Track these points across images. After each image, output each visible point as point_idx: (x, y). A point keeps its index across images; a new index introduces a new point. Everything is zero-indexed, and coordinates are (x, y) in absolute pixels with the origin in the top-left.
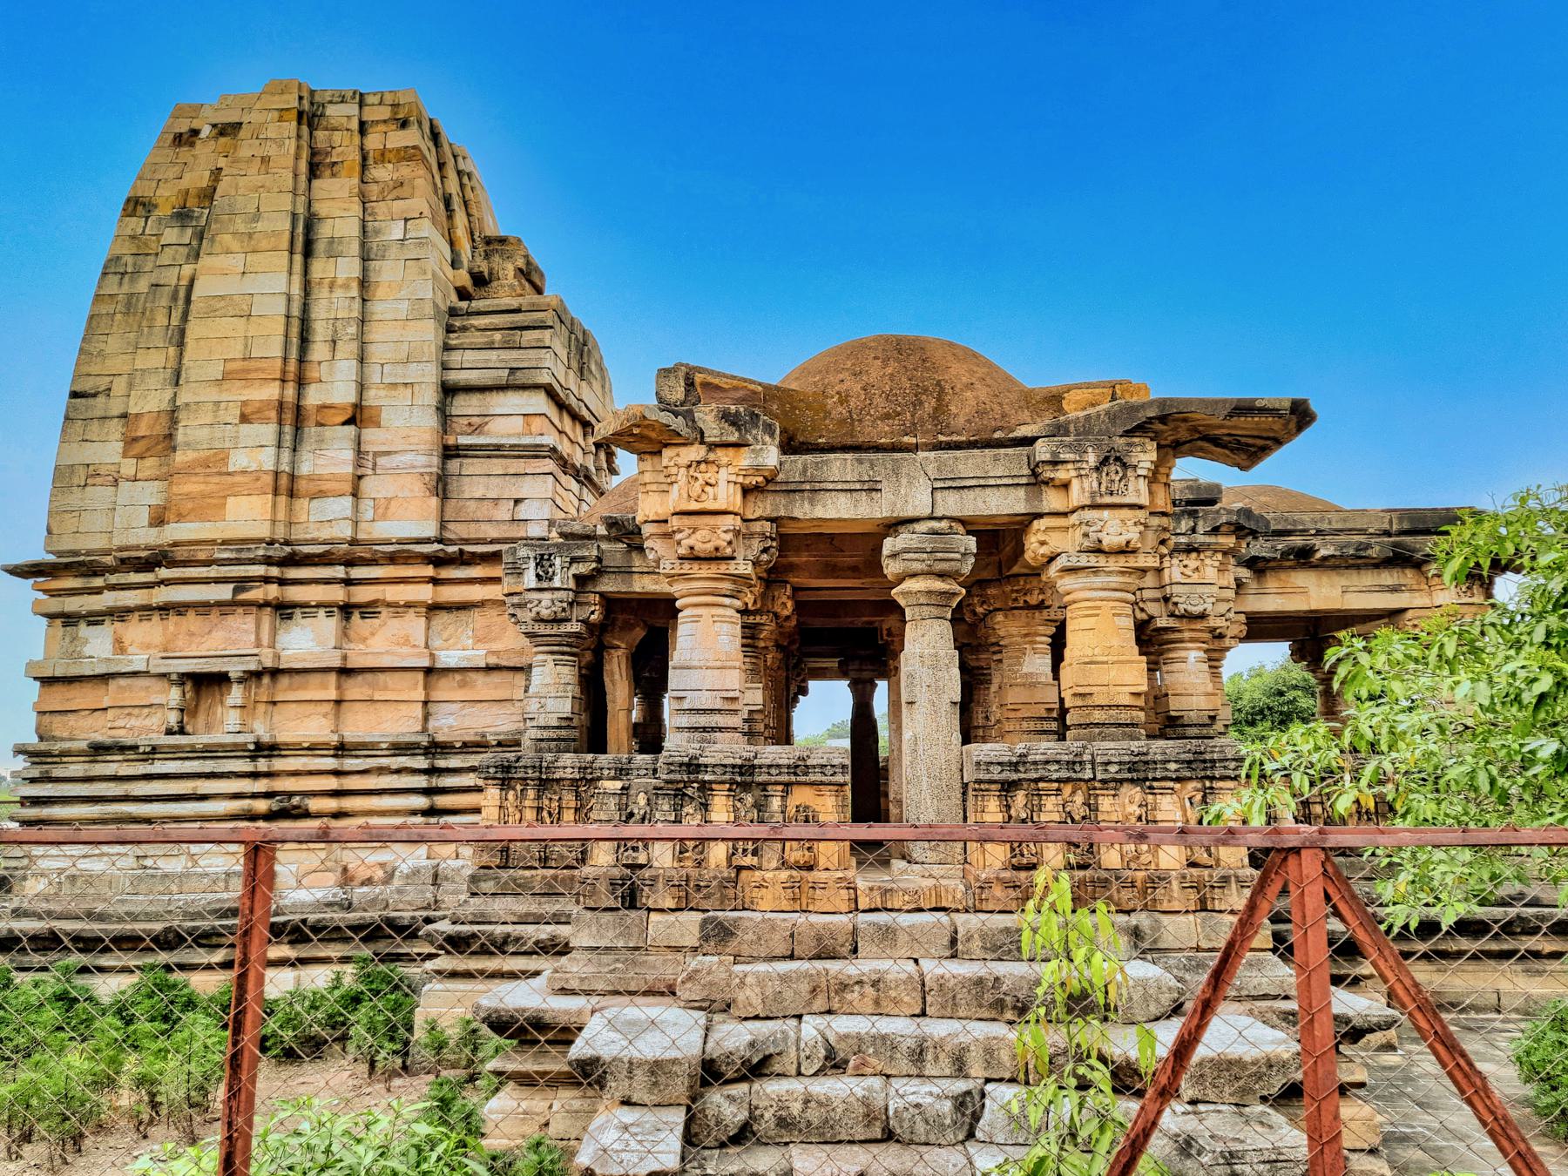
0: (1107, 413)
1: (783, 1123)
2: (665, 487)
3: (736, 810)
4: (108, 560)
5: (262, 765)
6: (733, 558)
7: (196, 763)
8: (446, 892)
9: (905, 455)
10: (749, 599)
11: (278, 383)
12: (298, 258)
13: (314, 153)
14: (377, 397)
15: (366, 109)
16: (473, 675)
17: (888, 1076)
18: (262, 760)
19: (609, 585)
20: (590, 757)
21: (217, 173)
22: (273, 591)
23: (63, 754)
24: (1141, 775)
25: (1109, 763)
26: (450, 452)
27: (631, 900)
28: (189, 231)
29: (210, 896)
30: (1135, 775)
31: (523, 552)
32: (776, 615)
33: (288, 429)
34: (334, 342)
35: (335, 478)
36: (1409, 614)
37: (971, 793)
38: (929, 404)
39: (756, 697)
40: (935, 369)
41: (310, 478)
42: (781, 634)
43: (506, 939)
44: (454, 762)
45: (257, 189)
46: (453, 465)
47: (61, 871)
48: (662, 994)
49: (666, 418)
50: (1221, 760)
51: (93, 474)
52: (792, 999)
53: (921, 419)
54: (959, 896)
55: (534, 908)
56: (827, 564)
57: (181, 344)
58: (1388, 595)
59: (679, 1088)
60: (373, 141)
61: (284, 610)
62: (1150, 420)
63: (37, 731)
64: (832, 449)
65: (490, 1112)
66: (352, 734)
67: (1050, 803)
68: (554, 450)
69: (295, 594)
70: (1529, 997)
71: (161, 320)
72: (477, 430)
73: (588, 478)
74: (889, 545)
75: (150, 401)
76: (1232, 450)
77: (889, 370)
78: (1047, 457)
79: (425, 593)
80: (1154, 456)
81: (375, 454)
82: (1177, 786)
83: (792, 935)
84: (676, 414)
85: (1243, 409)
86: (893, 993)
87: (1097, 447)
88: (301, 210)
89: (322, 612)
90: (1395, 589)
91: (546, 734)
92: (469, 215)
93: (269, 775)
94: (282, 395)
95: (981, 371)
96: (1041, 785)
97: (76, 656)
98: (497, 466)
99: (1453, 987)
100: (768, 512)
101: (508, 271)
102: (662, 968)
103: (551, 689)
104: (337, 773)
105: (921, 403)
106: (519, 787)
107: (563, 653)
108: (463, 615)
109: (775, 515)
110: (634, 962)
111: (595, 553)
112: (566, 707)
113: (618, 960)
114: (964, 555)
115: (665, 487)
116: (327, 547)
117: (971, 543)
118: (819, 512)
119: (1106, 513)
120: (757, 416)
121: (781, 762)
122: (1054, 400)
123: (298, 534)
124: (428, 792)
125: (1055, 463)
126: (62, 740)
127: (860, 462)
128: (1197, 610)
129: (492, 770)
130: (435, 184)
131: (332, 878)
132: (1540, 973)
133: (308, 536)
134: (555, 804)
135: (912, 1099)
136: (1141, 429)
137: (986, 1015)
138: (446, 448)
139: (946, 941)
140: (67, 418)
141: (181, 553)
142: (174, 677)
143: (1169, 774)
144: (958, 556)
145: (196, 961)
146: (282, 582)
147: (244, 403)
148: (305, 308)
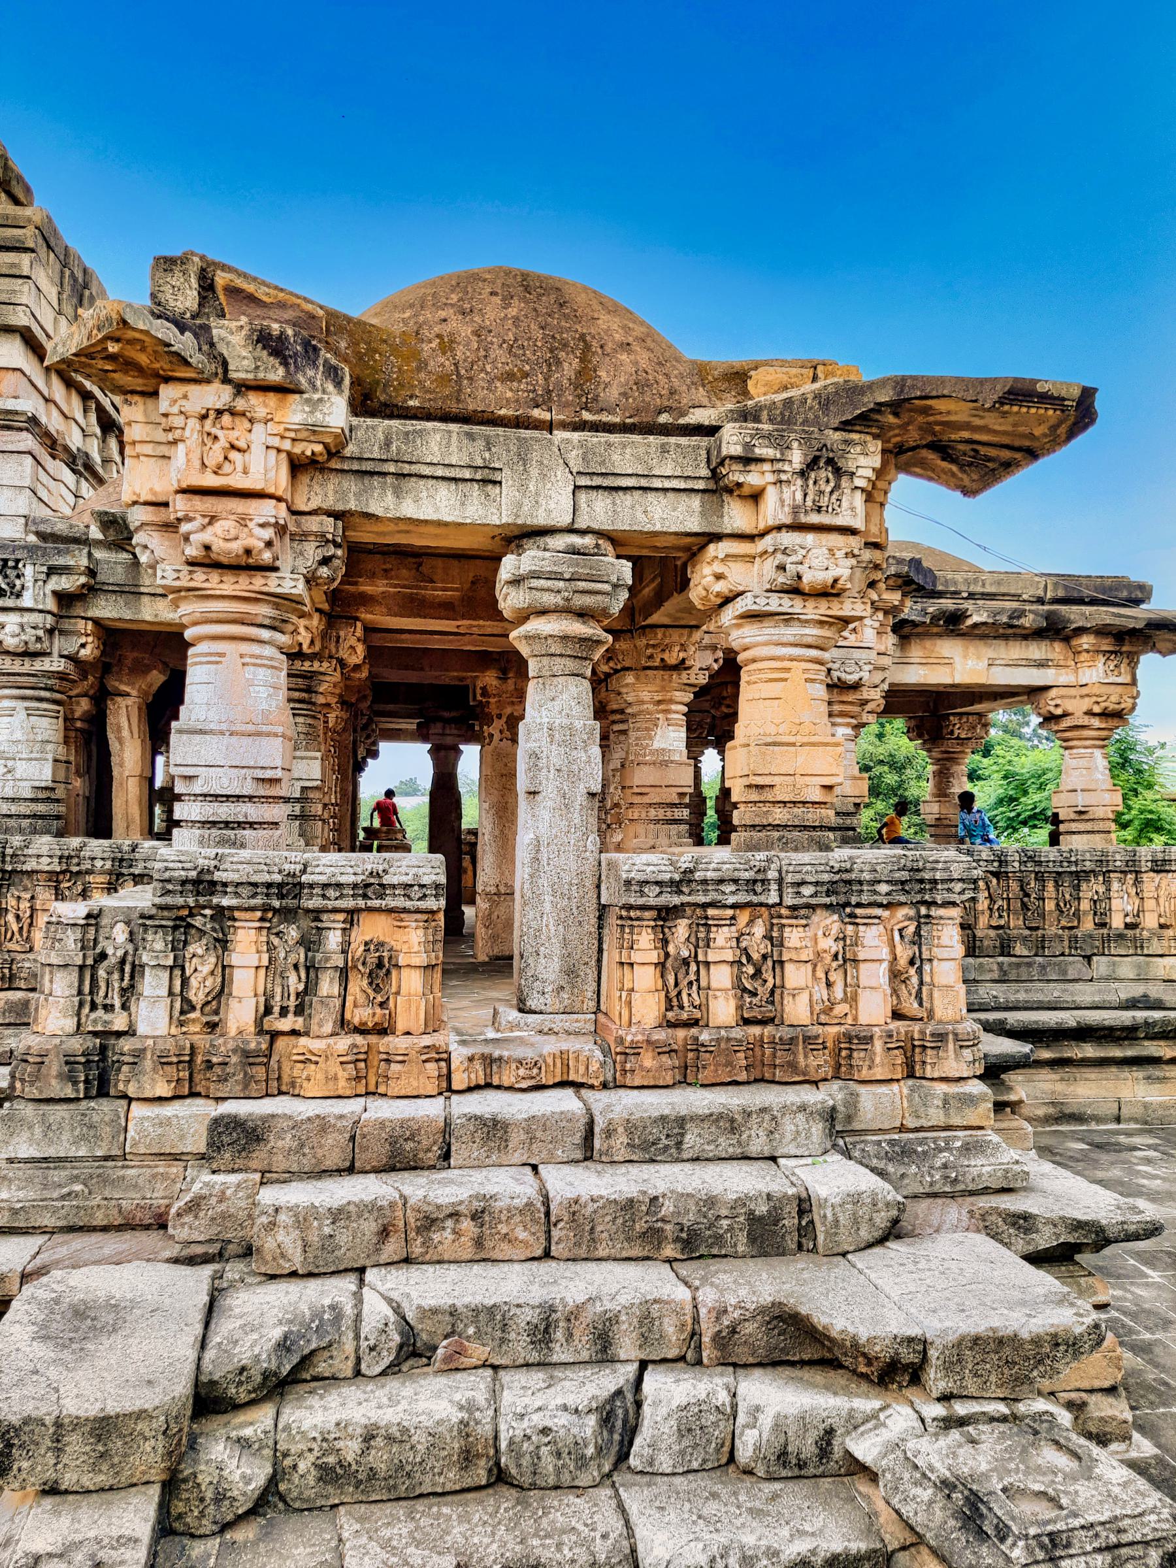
0: (817, 396)
1: (328, 1474)
2: (164, 450)
3: (271, 948)
6: (276, 569)
9: (536, 434)
10: (304, 638)
17: (495, 1368)
19: (106, 609)
24: (842, 899)
25: (799, 884)
27: (101, 1087)
30: (833, 899)
32: (341, 662)
36: (1053, 693)
37: (612, 921)
38: (570, 366)
39: (312, 768)
40: (578, 319)
48: (147, 1227)
49: (163, 330)
50: (943, 881)
52: (351, 1241)
53: (558, 383)
54: (594, 1067)
56: (412, 599)
58: (1034, 671)
59: (149, 1457)
62: (879, 407)
64: (429, 417)
67: (722, 936)
68: (34, 420)
70: (1146, 1106)
74: (509, 565)
76: (961, 467)
77: (512, 312)
78: (737, 450)
80: (877, 461)
82: (886, 914)
83: (353, 1138)
84: (182, 328)
85: (1020, 394)
86: (503, 1229)
87: (806, 440)
90: (1042, 664)
91: (14, 809)
95: (639, 331)
96: (711, 912)
99: (1076, 1096)
100: (330, 503)
102: (142, 1188)
105: (559, 362)
107: (40, 699)
109: (340, 507)
111: (84, 562)
113: (75, 1179)
114: (615, 586)
115: (164, 450)
117: (625, 569)
118: (409, 509)
119: (810, 538)
121: (343, 879)
122: (738, 378)
125: (747, 460)
127: (471, 437)
128: (851, 678)
132: (1163, 1080)
134: (24, 905)
135: (538, 1420)
136: (864, 421)
137: (636, 1252)
139: (578, 1138)
143: (879, 899)
144: (607, 587)
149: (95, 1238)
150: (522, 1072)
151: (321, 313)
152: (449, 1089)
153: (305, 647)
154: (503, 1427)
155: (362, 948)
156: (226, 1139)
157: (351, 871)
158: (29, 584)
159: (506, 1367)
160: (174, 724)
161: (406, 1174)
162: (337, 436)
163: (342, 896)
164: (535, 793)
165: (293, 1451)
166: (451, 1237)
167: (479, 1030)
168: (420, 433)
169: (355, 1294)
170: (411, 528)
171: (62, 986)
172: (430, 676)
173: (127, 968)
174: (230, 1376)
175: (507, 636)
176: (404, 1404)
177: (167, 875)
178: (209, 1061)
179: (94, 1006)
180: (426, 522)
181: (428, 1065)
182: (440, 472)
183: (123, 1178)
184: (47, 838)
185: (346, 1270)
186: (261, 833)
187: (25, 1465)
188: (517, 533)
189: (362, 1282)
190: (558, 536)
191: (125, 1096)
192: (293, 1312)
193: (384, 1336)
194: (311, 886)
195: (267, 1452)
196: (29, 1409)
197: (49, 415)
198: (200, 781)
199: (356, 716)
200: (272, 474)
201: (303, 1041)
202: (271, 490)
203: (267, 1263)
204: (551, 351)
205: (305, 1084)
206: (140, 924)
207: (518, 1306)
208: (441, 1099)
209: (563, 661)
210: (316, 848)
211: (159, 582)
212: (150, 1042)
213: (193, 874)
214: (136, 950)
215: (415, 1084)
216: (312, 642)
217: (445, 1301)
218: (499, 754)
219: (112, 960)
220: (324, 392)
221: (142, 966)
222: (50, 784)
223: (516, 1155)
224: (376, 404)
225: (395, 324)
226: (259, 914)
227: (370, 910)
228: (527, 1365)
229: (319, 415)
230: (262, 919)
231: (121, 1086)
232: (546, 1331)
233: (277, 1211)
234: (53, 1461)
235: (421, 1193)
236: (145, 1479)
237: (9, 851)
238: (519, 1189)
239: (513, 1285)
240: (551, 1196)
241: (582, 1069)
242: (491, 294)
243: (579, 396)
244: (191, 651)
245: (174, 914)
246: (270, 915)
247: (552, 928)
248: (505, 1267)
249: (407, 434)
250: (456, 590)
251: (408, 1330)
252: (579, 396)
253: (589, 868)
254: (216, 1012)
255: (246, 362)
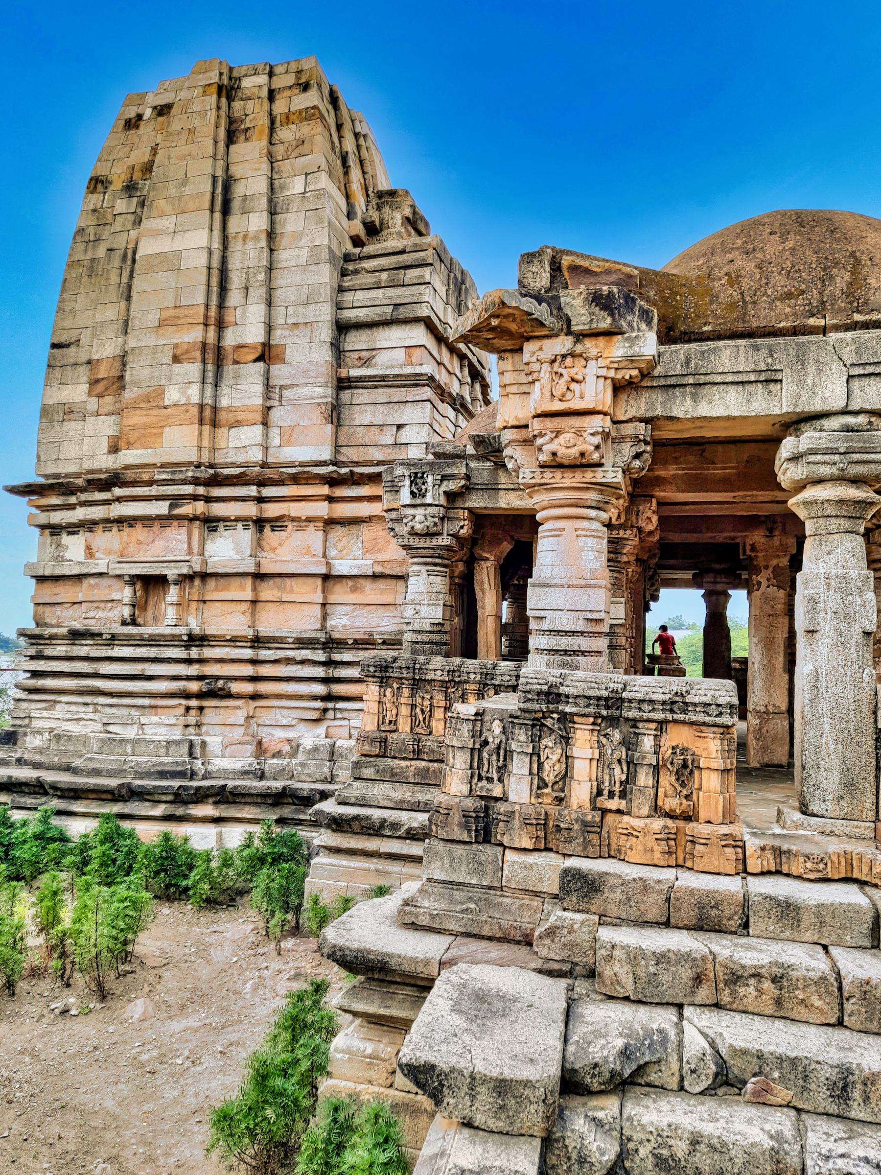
2: (525, 388)
3: (601, 746)
4: (80, 482)
5: (194, 653)
6: (601, 465)
7: (144, 649)
8: (341, 768)
11: (201, 327)
12: (218, 216)
13: (231, 121)
14: (282, 337)
15: (274, 78)
16: (362, 581)
17: (799, 1110)
18: (194, 649)
19: (477, 501)
20: (457, 660)
21: (154, 151)
22: (200, 507)
23: (52, 637)
26: (343, 384)
27: (485, 836)
28: (135, 200)
29: (154, 759)
31: (399, 471)
32: (640, 530)
33: (210, 367)
34: (247, 288)
35: (247, 409)
38: (842, 279)
41: (229, 409)
42: (642, 548)
43: (383, 822)
44: (347, 656)
45: (184, 157)
46: (346, 395)
47: (51, 730)
48: (518, 943)
49: (528, 305)
51: (69, 412)
53: (832, 295)
55: (408, 796)
57: (128, 299)
59: (533, 1117)
60: (280, 107)
61: (210, 523)
63: (35, 617)
64: (719, 337)
65: (336, 1050)
66: (265, 630)
68: (432, 378)
69: (219, 509)
71: (114, 278)
72: (366, 362)
73: (463, 405)
74: (788, 446)
75: (106, 349)
77: (790, 244)
79: (322, 509)
81: (282, 388)
83: (668, 900)
84: (540, 300)
88: (220, 173)
89: (240, 525)
91: (420, 638)
92: (364, 173)
93: (201, 661)
94: (205, 338)
97: (59, 559)
98: (382, 395)
100: (642, 412)
101: (396, 219)
102: (517, 914)
103: (425, 596)
104: (254, 662)
105: (832, 278)
106: (395, 685)
107: (435, 565)
108: (354, 529)
109: (650, 414)
110: (490, 904)
111: (464, 470)
112: (437, 614)
113: (470, 899)
115: (525, 388)
116: (242, 470)
118: (704, 410)
120: (633, 300)
121: (655, 697)
123: (220, 458)
124: (326, 681)
126: (52, 626)
127: (756, 348)
129: (372, 669)
130: (332, 143)
131: (250, 749)
133: (229, 460)
138: (340, 380)
140: (49, 366)
141: (130, 475)
142: (127, 578)
145: (143, 813)
146: (208, 500)
147: (176, 346)
148: (224, 260)
149: (484, 944)
150: (809, 865)
151: (636, 272)
152: (745, 871)
153: (613, 520)
154: (809, 1163)
155: (670, 751)
156: (573, 887)
157: (661, 690)
158: (430, 488)
159: (808, 1112)
160: (529, 580)
161: (713, 935)
162: (649, 361)
163: (654, 710)
164: (813, 632)
165: (635, 1138)
166: (754, 993)
167: (766, 825)
168: (714, 351)
169: (676, 1024)
170: (705, 424)
171: (460, 762)
172: (706, 537)
173: (502, 752)
174: (586, 1068)
175: (786, 502)
176: (722, 1123)
177: (528, 687)
178: (558, 826)
179: (480, 778)
180: (718, 418)
181: (726, 849)
182: (730, 378)
183: (502, 904)
184: (439, 658)
185: (668, 1004)
186: (590, 659)
187: (451, 1101)
188: (795, 418)
189: (681, 1016)
190: (833, 418)
191: (501, 845)
192: (629, 1029)
193: (702, 1064)
194: (630, 701)
195: (615, 1134)
196: (453, 1061)
197: (440, 374)
198: (547, 621)
199: (645, 570)
200: (601, 396)
201: (626, 818)
202: (600, 408)
203: (606, 986)
204: (825, 270)
205: (629, 852)
206: (510, 721)
207: (818, 1063)
208: (738, 879)
209: (838, 521)
210: (622, 671)
211: (521, 481)
212: (517, 807)
213: (545, 688)
214: (507, 740)
215: (716, 863)
216: (619, 517)
217: (755, 1046)
218: (766, 598)
219: (492, 746)
220: (639, 330)
221: (512, 752)
222: (441, 621)
223: (808, 934)
224: (677, 333)
225: (690, 271)
226: (592, 719)
227: (676, 722)
228: (827, 1114)
229: (636, 348)
230: (594, 724)
231: (499, 837)
232: (844, 1088)
233: (613, 947)
234: (469, 1104)
235: (727, 953)
236: (530, 1132)
237: (417, 666)
238: (813, 964)
239: (810, 1042)
240: (843, 973)
241: (865, 870)
242: (771, 233)
243: (851, 303)
244: (541, 529)
245: (532, 716)
246: (599, 721)
247: (832, 747)
248: (804, 1028)
249: (703, 353)
250: (732, 468)
251: (722, 1065)
252: (851, 303)
253: (866, 695)
254: (562, 790)
255: (584, 318)
